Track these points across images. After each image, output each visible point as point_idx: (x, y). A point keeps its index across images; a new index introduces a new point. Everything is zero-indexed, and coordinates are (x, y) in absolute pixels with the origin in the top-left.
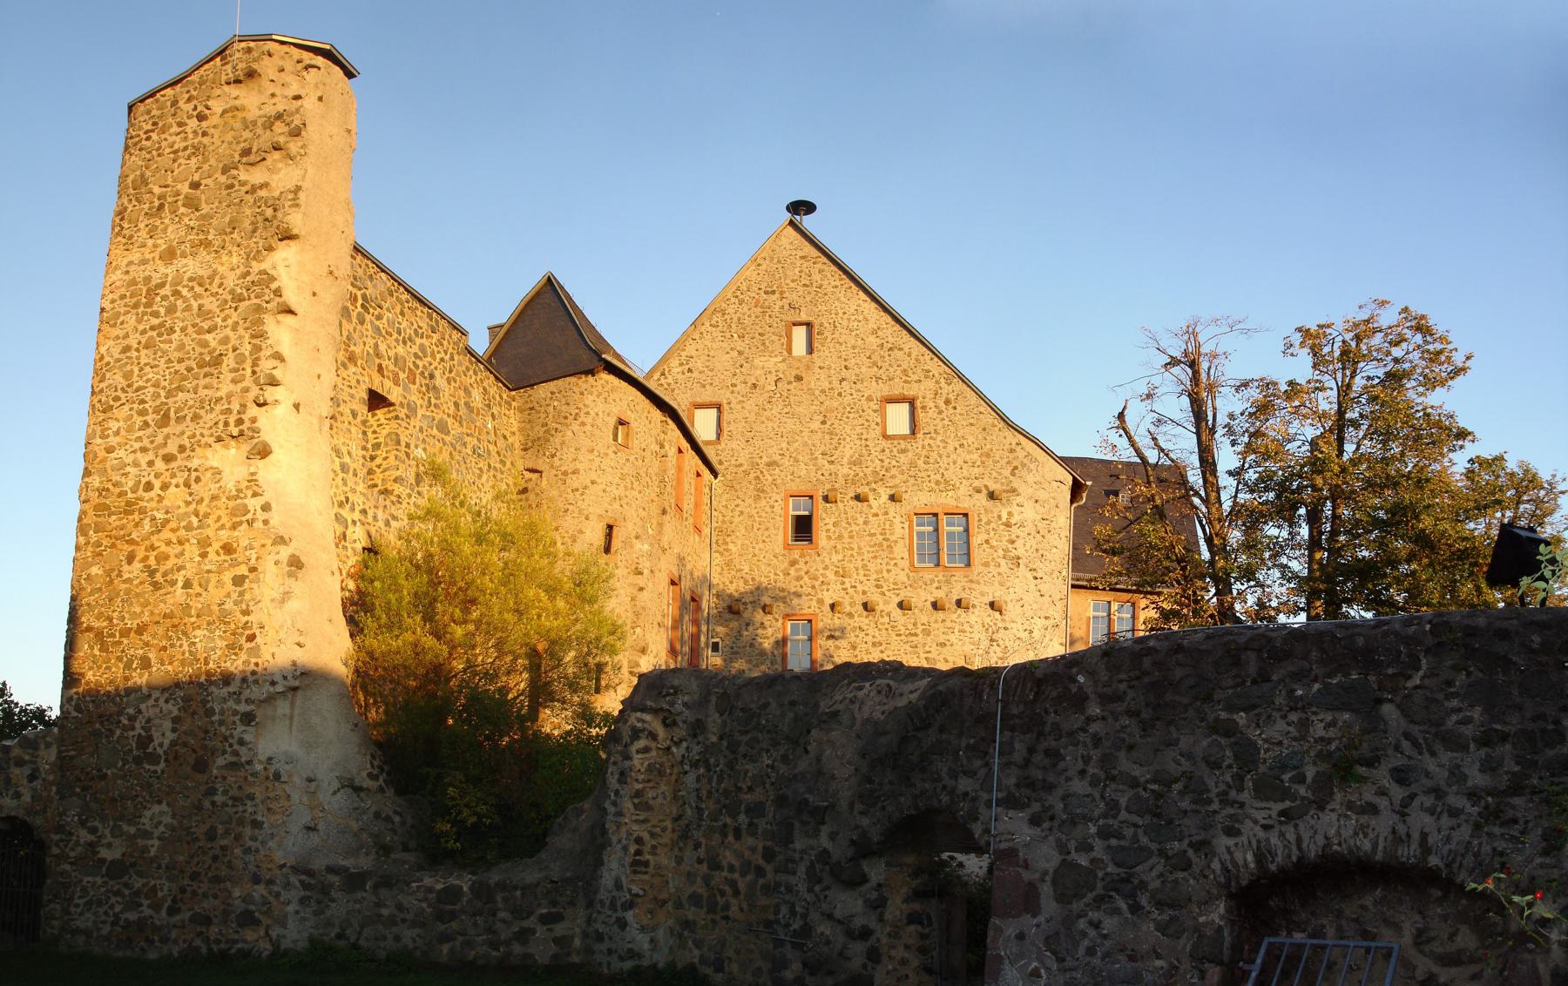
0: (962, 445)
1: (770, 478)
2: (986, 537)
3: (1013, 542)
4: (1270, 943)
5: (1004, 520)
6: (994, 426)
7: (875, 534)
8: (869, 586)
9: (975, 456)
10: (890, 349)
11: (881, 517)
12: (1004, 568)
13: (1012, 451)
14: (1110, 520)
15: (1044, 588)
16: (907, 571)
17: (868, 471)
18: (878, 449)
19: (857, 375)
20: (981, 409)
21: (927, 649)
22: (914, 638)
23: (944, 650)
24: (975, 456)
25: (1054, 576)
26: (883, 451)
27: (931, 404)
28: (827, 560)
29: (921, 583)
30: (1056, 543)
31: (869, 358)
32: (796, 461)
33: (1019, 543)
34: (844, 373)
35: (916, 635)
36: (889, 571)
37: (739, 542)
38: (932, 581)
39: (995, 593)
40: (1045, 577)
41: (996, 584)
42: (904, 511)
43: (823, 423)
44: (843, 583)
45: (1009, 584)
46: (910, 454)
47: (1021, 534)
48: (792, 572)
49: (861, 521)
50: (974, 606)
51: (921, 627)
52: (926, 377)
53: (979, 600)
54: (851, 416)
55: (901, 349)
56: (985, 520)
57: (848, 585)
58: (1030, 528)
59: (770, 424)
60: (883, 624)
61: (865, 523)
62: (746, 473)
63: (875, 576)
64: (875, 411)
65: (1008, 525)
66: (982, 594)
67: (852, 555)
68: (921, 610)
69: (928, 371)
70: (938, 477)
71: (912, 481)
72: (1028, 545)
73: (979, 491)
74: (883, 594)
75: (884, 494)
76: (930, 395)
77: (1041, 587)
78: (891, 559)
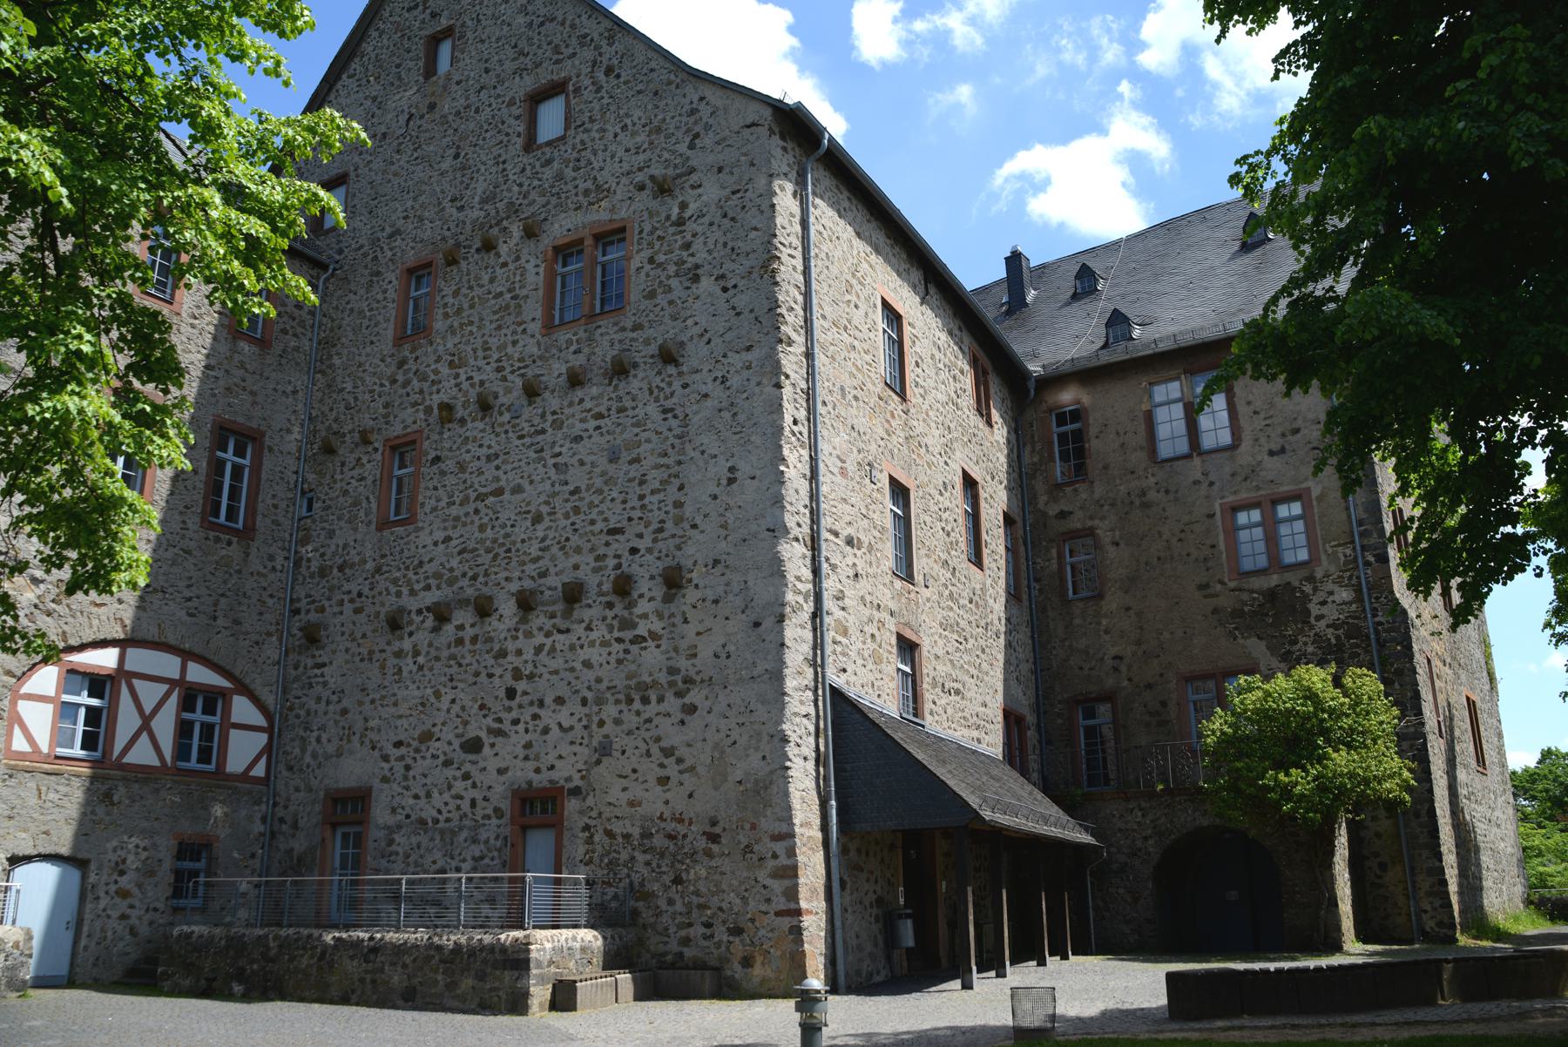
0: (625, 128)
1: (389, 254)
2: (646, 253)
3: (687, 246)
4: (209, 762)
5: (674, 217)
6: (670, 83)
7: (501, 294)
8: (489, 373)
9: (641, 138)
10: (542, 24)
11: (511, 266)
12: (678, 291)
13: (693, 112)
14: (58, 481)
15: (741, 301)
16: (538, 336)
17: (501, 206)
18: (517, 170)
19: (498, 76)
20: (653, 64)
21: (557, 449)
22: (540, 438)
23: (579, 447)
24: (641, 138)
25: (755, 275)
26: (523, 170)
27: (587, 82)
28: (441, 348)
29: (554, 351)
30: (754, 222)
31: (516, 46)
32: (421, 219)
33: (697, 245)
34: (485, 79)
35: (543, 431)
36: (515, 343)
37: (345, 351)
38: (569, 342)
39: (666, 331)
40: (742, 283)
41: (667, 320)
42: (541, 247)
43: (456, 156)
44: (457, 376)
45: (684, 314)
46: (556, 165)
47: (699, 229)
48: (400, 378)
49: (486, 278)
50: (635, 365)
51: (550, 418)
52: (582, 45)
53: (644, 353)
54: (488, 135)
55: (553, 20)
56: (647, 228)
57: (463, 377)
58: (714, 214)
59: (396, 181)
60: (502, 425)
61: (492, 281)
62: (365, 255)
63: (495, 357)
64: (517, 118)
65: (680, 222)
66: (647, 342)
67: (471, 333)
68: (553, 392)
69: (585, 36)
70: (589, 184)
71: (554, 200)
72: (711, 242)
73: (641, 188)
74: (504, 379)
75: (516, 230)
76: (585, 70)
77: (734, 301)
78: (520, 324)
